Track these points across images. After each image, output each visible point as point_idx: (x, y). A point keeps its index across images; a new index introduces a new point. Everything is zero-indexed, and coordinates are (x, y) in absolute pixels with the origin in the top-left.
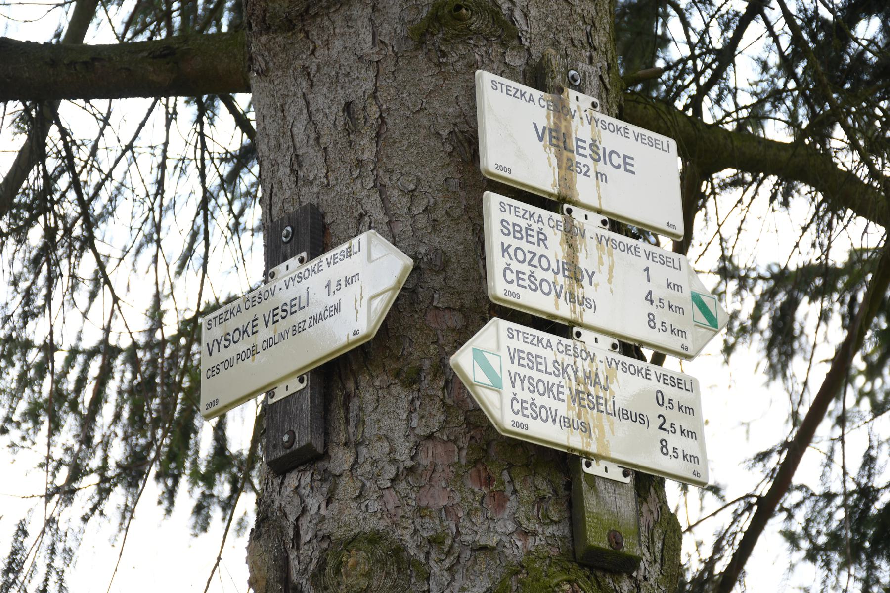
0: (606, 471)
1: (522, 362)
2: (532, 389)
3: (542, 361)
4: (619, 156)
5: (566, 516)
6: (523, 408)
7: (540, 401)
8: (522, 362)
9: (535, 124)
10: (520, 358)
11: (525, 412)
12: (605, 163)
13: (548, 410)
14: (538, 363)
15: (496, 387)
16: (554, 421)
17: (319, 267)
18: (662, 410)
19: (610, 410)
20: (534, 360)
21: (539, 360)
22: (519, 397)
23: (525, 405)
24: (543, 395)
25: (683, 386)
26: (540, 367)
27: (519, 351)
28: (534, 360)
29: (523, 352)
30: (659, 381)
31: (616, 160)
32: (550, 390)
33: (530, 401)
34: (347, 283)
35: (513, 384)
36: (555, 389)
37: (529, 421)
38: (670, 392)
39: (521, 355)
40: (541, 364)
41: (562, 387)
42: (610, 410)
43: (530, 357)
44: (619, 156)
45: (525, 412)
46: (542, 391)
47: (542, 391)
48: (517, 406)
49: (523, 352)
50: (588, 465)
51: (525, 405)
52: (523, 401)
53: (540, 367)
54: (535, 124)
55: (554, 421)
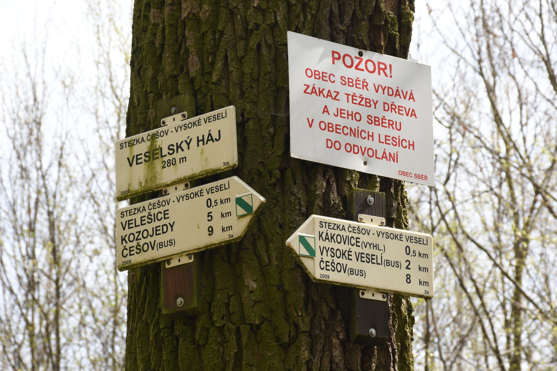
0: (373, 296)
1: (363, 259)
2: (333, 255)
3: (375, 257)
4: (406, 142)
5: (303, 296)
6: (327, 266)
7: (336, 260)
8: (363, 259)
9: (308, 119)
10: (362, 257)
11: (328, 268)
12: (399, 146)
13: (342, 265)
14: (372, 259)
15: (312, 253)
16: (345, 272)
17: (201, 193)
18: (408, 257)
19: (379, 262)
20: (370, 258)
21: (373, 257)
22: (324, 260)
23: (328, 264)
24: (339, 258)
25: (422, 242)
26: (373, 261)
27: (362, 253)
28: (370, 258)
29: (364, 254)
30: (407, 241)
31: (405, 144)
32: (344, 254)
33: (331, 261)
34: (221, 202)
35: (322, 254)
36: (346, 254)
37: (330, 273)
38: (414, 247)
39: (363, 255)
40: (374, 259)
41: (351, 252)
42: (379, 262)
43: (368, 256)
44: (406, 142)
45: (328, 268)
46: (338, 256)
47: (338, 256)
48: (323, 265)
49: (364, 254)
50: (363, 294)
51: (328, 264)
52: (327, 262)
53: (373, 261)
54: (308, 119)
55: (345, 272)
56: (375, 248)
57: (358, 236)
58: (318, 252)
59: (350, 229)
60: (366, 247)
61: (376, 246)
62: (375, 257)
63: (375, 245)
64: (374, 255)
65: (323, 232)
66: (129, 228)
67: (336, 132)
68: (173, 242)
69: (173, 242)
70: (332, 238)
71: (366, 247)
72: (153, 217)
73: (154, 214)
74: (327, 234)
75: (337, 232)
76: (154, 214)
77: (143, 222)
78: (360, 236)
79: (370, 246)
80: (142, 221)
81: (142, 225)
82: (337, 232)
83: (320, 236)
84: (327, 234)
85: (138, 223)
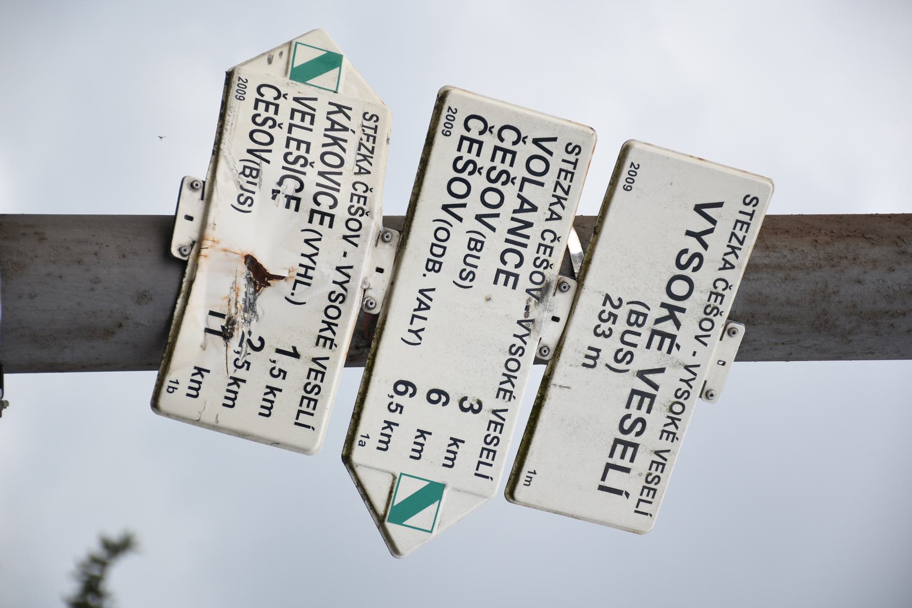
11: (262, 106)
35: (296, 99)
48: (269, 95)
56: (302, 271)
57: (339, 224)
58: (304, 90)
59: (361, 189)
60: (307, 241)
61: (305, 276)
62: (307, 123)
63: (310, 273)
64: (312, 123)
65: (349, 118)
66: (293, 111)
67: (617, 441)
68: (245, 207)
69: (245, 207)
70: (336, 141)
71: (307, 241)
72: (297, 167)
73: (304, 174)
74: (345, 129)
75: (350, 157)
76: (304, 174)
77: (293, 144)
78: (340, 228)
79: (309, 257)
80: (299, 142)
81: (289, 139)
82: (350, 157)
83: (341, 109)
84: (345, 129)
85: (297, 133)
